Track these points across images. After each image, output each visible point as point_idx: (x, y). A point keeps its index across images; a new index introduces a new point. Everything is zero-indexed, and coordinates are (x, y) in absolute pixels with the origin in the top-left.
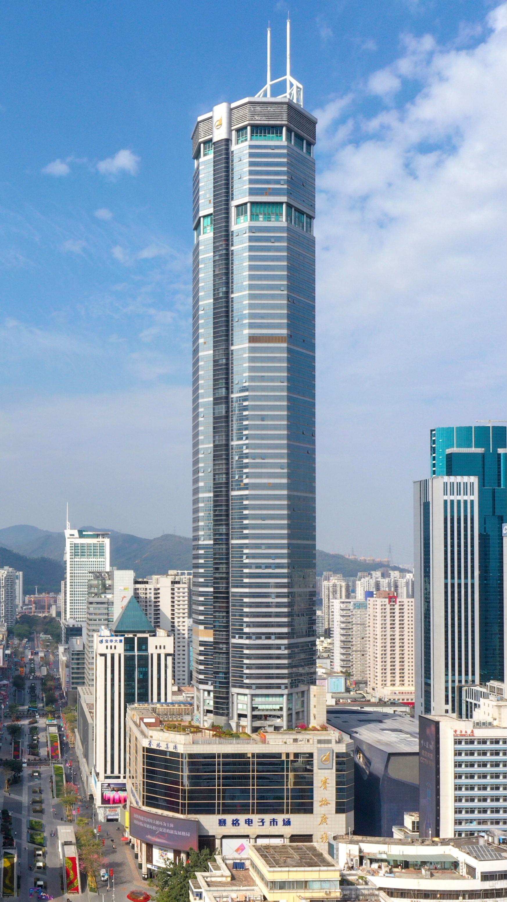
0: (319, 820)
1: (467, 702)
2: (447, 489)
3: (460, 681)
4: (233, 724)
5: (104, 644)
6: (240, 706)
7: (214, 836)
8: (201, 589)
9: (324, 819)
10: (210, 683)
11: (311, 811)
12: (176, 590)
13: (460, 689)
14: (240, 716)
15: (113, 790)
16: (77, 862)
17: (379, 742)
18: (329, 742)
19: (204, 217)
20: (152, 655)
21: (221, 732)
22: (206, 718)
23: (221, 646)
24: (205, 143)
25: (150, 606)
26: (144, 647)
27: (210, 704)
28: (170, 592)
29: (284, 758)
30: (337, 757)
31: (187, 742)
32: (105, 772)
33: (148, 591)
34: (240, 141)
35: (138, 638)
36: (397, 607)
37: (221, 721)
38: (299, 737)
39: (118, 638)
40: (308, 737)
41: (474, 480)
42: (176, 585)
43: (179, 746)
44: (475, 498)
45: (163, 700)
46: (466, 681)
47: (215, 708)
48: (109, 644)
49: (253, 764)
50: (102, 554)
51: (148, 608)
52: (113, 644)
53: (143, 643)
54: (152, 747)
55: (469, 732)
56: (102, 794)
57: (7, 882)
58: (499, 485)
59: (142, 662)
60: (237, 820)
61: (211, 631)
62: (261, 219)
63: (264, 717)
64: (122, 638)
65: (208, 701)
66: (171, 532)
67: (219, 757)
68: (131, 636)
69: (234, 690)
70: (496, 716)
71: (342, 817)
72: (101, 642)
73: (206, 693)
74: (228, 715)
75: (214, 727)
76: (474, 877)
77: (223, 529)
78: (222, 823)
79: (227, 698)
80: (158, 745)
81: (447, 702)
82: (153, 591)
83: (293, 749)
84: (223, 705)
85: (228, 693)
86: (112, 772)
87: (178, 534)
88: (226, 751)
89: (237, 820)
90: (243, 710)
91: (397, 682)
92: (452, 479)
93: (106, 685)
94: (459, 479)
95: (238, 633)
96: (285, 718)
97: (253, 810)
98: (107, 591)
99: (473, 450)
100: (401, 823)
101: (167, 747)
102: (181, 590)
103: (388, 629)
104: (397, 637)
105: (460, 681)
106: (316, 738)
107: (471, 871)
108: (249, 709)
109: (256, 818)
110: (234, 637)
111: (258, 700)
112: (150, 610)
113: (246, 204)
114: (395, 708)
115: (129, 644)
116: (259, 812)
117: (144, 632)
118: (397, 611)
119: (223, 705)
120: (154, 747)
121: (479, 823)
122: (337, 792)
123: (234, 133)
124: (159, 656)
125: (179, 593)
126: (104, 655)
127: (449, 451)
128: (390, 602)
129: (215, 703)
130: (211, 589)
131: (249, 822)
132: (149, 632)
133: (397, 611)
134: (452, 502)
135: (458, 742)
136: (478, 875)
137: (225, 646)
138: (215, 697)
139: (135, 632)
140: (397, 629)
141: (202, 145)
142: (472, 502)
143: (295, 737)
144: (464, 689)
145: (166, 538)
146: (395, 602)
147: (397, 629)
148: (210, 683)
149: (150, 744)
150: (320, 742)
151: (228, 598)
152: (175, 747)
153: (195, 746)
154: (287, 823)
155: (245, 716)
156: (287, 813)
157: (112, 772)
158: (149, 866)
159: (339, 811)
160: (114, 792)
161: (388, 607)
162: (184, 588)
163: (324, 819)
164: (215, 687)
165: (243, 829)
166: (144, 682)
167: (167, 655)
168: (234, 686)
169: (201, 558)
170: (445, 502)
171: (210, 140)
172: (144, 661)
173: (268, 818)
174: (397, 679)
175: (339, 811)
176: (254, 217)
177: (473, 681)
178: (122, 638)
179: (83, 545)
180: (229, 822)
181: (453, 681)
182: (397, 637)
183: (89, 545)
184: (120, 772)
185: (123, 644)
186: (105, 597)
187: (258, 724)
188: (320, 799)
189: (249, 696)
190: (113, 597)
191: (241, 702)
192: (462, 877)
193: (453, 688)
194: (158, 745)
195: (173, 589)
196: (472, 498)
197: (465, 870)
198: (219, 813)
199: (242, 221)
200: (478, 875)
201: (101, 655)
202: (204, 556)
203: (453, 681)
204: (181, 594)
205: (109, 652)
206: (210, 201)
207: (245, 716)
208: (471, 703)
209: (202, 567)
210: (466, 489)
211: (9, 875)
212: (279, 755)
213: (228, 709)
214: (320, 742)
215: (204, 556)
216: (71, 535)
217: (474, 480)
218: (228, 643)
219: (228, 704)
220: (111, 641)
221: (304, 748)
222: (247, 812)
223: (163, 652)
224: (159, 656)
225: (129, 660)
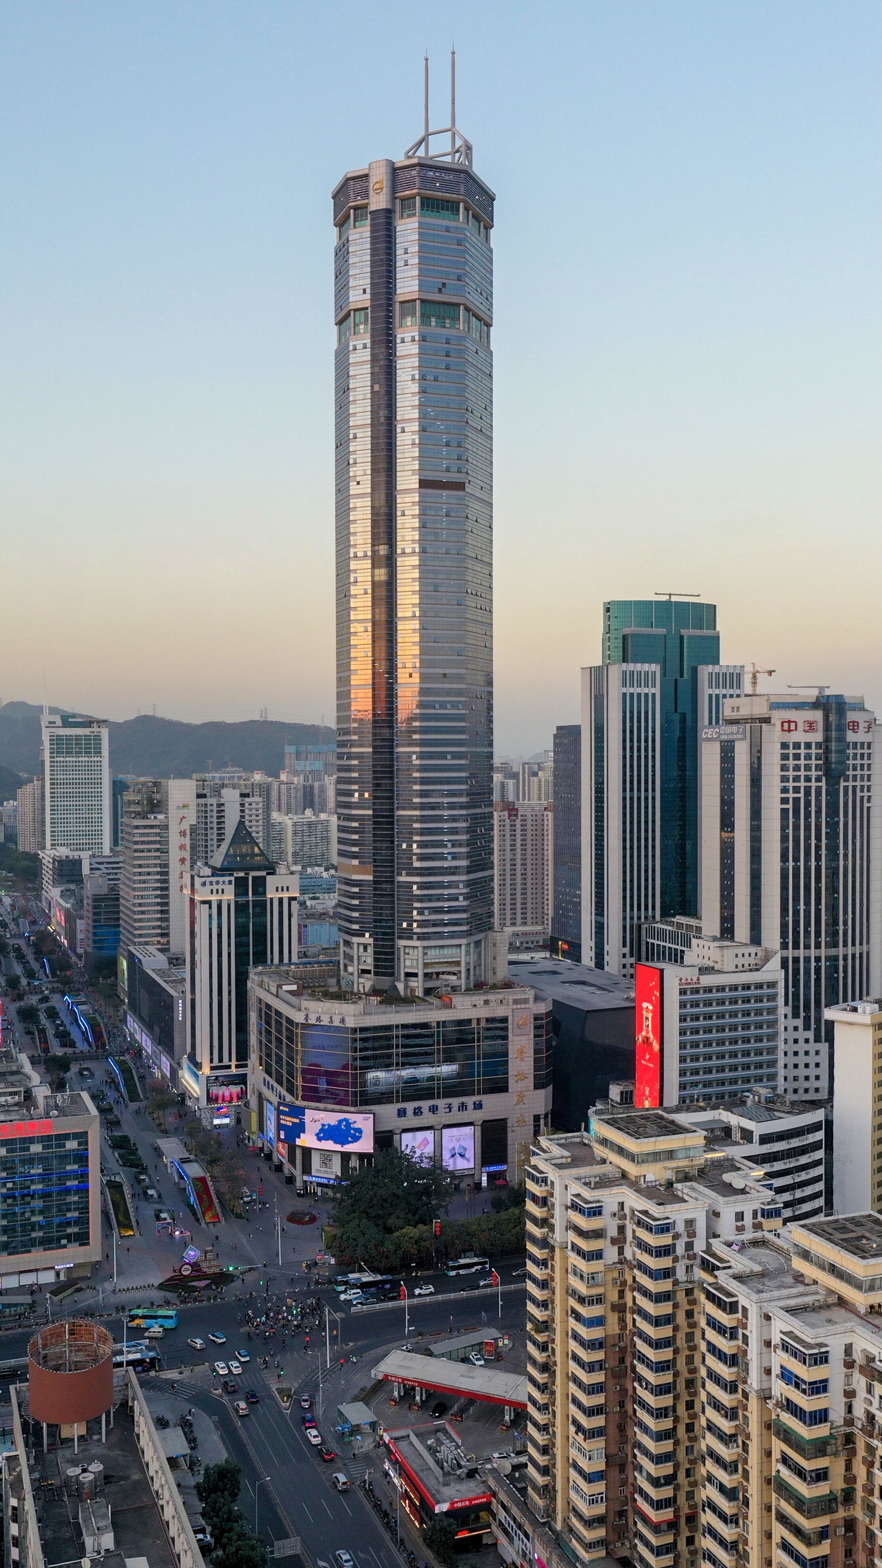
0: (516, 1098)
1: (647, 943)
2: (627, 679)
3: (639, 918)
4: (400, 986)
5: (208, 888)
6: (408, 963)
7: (391, 1131)
8: (354, 812)
9: (521, 1100)
10: (367, 935)
11: (507, 1091)
12: (247, 805)
13: (639, 927)
14: (408, 975)
15: (223, 1084)
16: (210, 1184)
17: (568, 998)
18: (526, 1001)
19: (355, 310)
20: (271, 899)
21: (389, 997)
22: (361, 980)
23: (384, 886)
24: (356, 208)
25: (212, 828)
26: (261, 889)
27: (369, 962)
28: (239, 808)
29: (474, 1024)
30: (535, 1019)
31: (357, 1013)
32: (211, 1061)
33: (209, 808)
34: (405, 215)
35: (254, 878)
36: (518, 822)
37: (384, 982)
38: (491, 997)
39: (227, 879)
40: (500, 997)
41: (655, 668)
42: (247, 799)
43: (347, 1019)
44: (657, 690)
45: (286, 960)
46: (646, 918)
47: (376, 966)
48: (215, 887)
49: (397, 1037)
50: (99, 753)
51: (209, 832)
52: (220, 887)
53: (260, 883)
54: (310, 1022)
55: (695, 980)
56: (208, 1091)
57: (121, 1218)
58: (682, 675)
59: (258, 910)
60: (419, 1108)
61: (370, 867)
62: (433, 324)
63: (435, 976)
64: (232, 878)
65: (363, 959)
66: (150, 713)
67: (397, 1027)
68: (241, 874)
69: (402, 943)
70: (718, 959)
71: (541, 1093)
72: (204, 884)
73: (361, 949)
74: (392, 974)
75: (375, 992)
76: (751, 1141)
77: (386, 732)
78: (402, 1113)
79: (393, 953)
80: (319, 1019)
81: (624, 946)
82: (215, 808)
83: (484, 1013)
84: (386, 962)
85: (393, 946)
86: (221, 1060)
87: (159, 715)
88: (406, 1022)
89: (419, 1108)
90: (411, 967)
91: (519, 921)
92: (631, 667)
93: (211, 944)
94: (639, 667)
95: (404, 869)
96: (463, 975)
97: (439, 1093)
98: (158, 809)
99: (654, 631)
100: (604, 1095)
101: (331, 1021)
102: (254, 806)
103: (508, 852)
104: (519, 862)
105: (639, 918)
106: (511, 998)
107: (747, 1135)
108: (421, 966)
109: (441, 1103)
110: (400, 874)
111: (432, 953)
112: (212, 834)
113: (415, 300)
114: (533, 955)
115: (241, 886)
116: (446, 1096)
117: (259, 869)
118: (518, 828)
119: (386, 962)
120: (312, 1021)
121: (704, 1086)
122: (535, 1062)
123: (398, 201)
124: (281, 900)
125: (251, 810)
126: (209, 903)
127: (627, 631)
128: (510, 815)
129: (376, 960)
130: (370, 812)
131: (434, 1109)
132: (265, 868)
133: (518, 828)
134: (632, 695)
135: (683, 992)
136: (756, 1138)
137: (389, 886)
138: (375, 953)
139: (247, 869)
140: (519, 852)
141: (352, 211)
142: (654, 695)
143: (485, 998)
144: (644, 926)
145: (143, 720)
146: (516, 815)
147: (519, 852)
148: (367, 935)
149: (306, 1019)
150: (516, 1002)
151: (392, 823)
152: (343, 1021)
153: (368, 1017)
154: (478, 1106)
155: (415, 975)
156: (479, 1094)
157: (221, 1060)
158: (306, 1178)
159: (536, 1087)
160: (224, 1087)
161: (508, 822)
162: (257, 803)
163: (521, 1100)
164: (375, 940)
165: (427, 1118)
166: (261, 936)
167: (291, 899)
168: (400, 938)
169: (354, 771)
170: (624, 695)
171: (365, 207)
172: (261, 906)
173: (455, 1102)
174: (519, 916)
175: (536, 1087)
176: (425, 318)
177: (654, 917)
178: (232, 878)
179: (69, 738)
180: (410, 1112)
181: (632, 918)
182: (519, 862)
183: (78, 738)
184: (230, 1060)
185: (233, 886)
186: (155, 818)
187: (430, 984)
188: (515, 1073)
189: (420, 949)
190: (167, 817)
191: (412, 956)
192: (737, 1143)
193: (631, 927)
194: (319, 1019)
195: (242, 805)
196: (653, 690)
197: (739, 1135)
198: (397, 1102)
199: (409, 323)
200: (756, 1138)
201: (204, 902)
202: (358, 768)
203: (632, 918)
204: (254, 811)
205: (214, 898)
206: (364, 291)
207: (415, 975)
208: (653, 944)
209: (355, 783)
210: (646, 679)
211: (122, 1208)
212: (469, 1021)
213: (393, 967)
214: (516, 1002)
215: (358, 768)
216: (50, 723)
217: (655, 668)
218: (392, 882)
219: (393, 960)
220: (217, 883)
221: (500, 1012)
222: (431, 1096)
223: (285, 895)
224: (281, 900)
225: (241, 908)
